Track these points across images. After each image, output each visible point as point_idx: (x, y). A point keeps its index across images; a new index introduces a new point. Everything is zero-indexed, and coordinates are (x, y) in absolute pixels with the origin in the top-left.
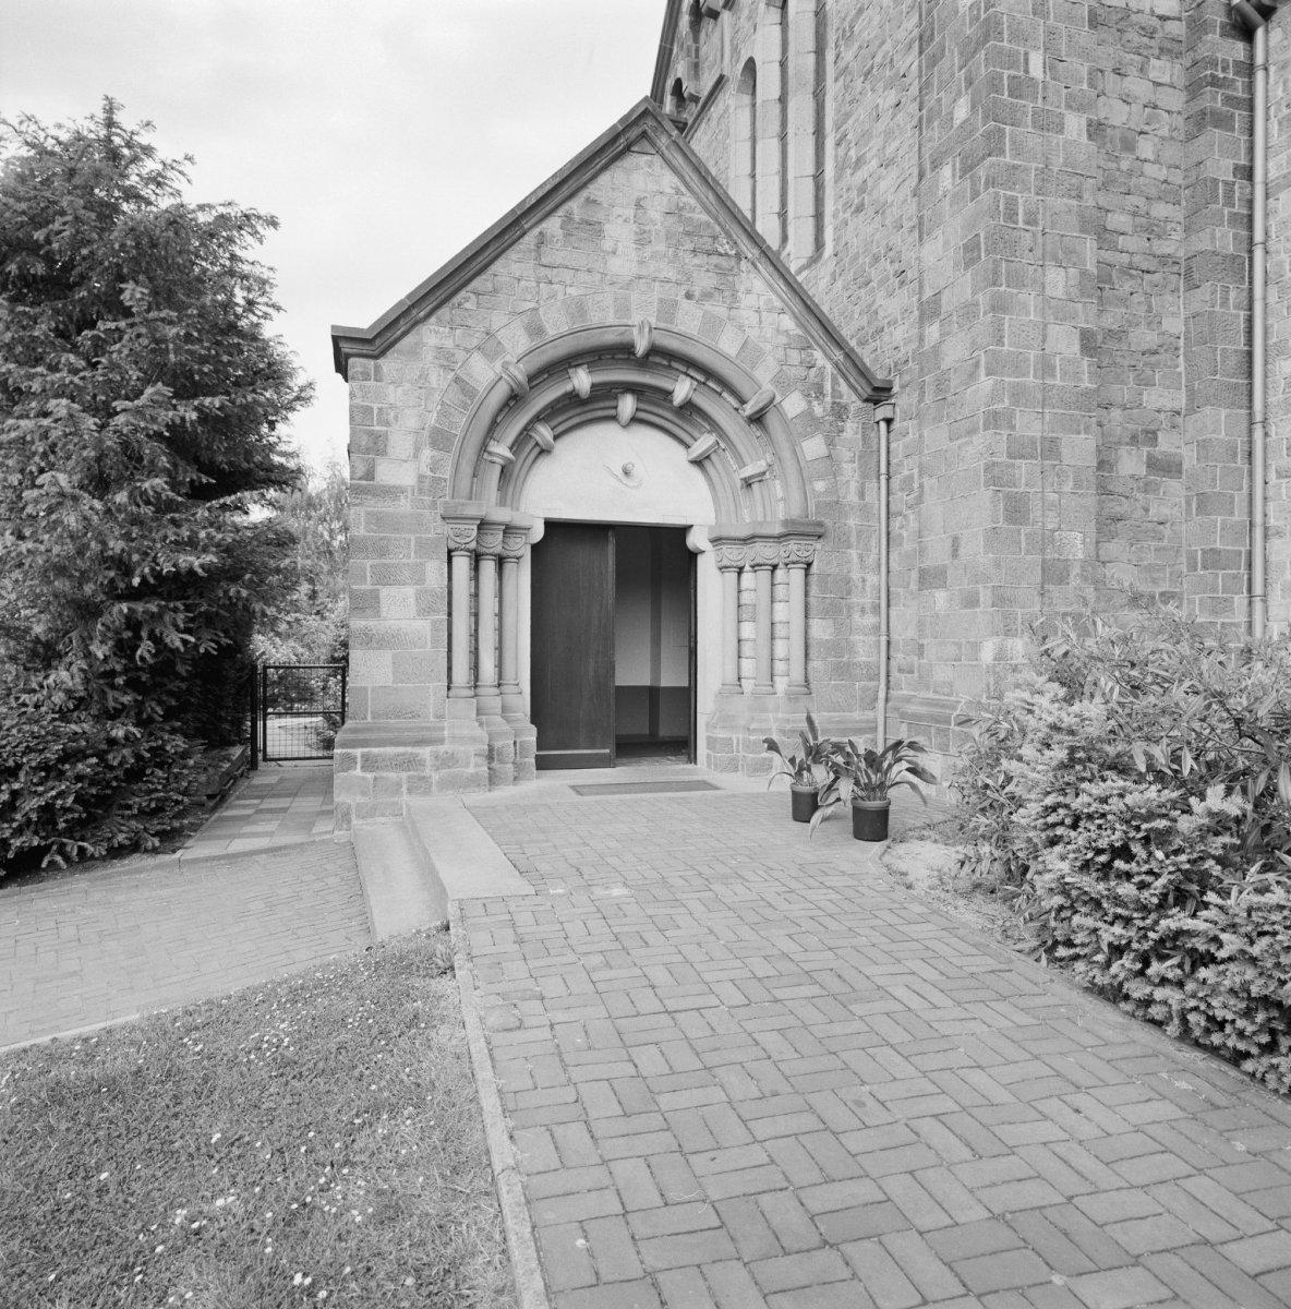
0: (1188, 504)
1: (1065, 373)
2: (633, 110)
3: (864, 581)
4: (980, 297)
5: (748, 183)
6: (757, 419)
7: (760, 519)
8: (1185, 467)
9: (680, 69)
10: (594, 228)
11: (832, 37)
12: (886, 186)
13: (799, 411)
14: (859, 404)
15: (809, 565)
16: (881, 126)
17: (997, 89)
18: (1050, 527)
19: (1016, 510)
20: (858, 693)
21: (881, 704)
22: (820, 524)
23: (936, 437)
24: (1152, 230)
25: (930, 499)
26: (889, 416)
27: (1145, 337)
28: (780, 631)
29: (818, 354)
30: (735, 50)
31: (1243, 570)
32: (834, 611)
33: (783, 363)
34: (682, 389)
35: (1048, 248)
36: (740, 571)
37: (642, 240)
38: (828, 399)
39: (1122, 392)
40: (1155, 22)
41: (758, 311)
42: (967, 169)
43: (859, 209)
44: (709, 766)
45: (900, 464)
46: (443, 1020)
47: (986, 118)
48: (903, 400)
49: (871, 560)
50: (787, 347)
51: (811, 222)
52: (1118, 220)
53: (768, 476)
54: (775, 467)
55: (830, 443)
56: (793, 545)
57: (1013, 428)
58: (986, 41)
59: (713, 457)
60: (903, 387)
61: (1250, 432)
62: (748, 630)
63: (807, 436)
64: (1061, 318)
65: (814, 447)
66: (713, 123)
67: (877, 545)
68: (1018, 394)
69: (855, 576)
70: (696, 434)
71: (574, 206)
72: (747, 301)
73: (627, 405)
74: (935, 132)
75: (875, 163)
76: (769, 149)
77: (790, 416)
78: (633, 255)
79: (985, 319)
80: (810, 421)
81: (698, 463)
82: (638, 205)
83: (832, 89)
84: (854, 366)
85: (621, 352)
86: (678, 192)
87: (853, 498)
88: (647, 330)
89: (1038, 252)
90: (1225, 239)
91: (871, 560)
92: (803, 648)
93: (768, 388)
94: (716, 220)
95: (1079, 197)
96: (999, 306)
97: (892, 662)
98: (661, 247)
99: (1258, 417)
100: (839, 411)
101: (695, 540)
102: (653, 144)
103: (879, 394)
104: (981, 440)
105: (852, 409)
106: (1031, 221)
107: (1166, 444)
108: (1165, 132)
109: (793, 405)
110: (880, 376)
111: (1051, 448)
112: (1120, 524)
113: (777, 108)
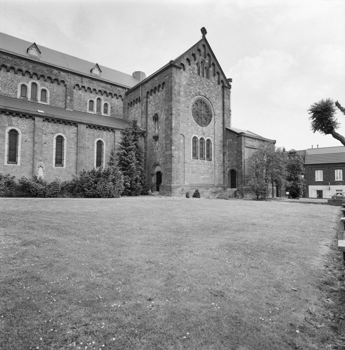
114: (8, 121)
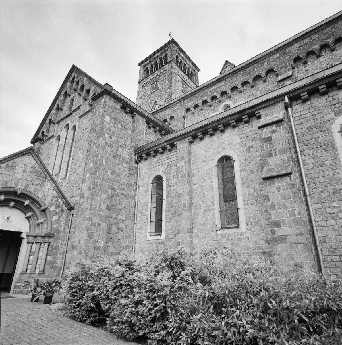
0: (124, 236)
1: (103, 212)
2: (29, 148)
3: (62, 247)
4: (90, 196)
5: (54, 158)
6: (44, 211)
7: (40, 232)
8: (124, 230)
9: (44, 129)
10: (13, 168)
11: (75, 141)
12: (79, 170)
13: (53, 210)
14: (67, 210)
15: (49, 243)
16: (80, 160)
17: (97, 164)
18: (97, 239)
19: (91, 236)
20: (56, 273)
21: (60, 276)
22: (54, 234)
23: (79, 220)
24: (121, 189)
25: (76, 232)
26: (73, 213)
27: (119, 207)
28: (40, 258)
29: (60, 199)
30: (57, 132)
31: (131, 249)
32: (53, 254)
33: (52, 200)
34: (27, 202)
35: (103, 190)
36: (33, 243)
37: (24, 171)
38: (60, 208)
39: (114, 216)
40: (125, 158)
41: (48, 189)
42: (91, 175)
43: (74, 172)
44: (13, 293)
45: (73, 223)
46: (133, 117)
47: (95, 168)
48: (76, 211)
49: (64, 243)
50: (53, 197)
51: (66, 170)
52: (116, 187)
53: (44, 223)
54: (46, 221)
55: (59, 217)
56: (46, 239)
57: (92, 220)
58: (96, 156)
59: (32, 217)
60: (76, 208)
61: (134, 225)
62: (31, 258)
63: (54, 215)
64: (104, 202)
65: (55, 218)
66: (50, 143)
67: (66, 241)
68: (94, 215)
69: (60, 246)
70: (28, 212)
71: (10, 163)
72: (46, 187)
73: (12, 204)
74: (87, 166)
75: (78, 166)
76: (60, 154)
77: (51, 211)
78: (22, 174)
79: (90, 201)
80: (55, 213)
81: (28, 218)
82: (25, 165)
83: (73, 149)
84: (67, 203)
85: (14, 193)
86: (35, 164)
87: (62, 229)
88: (21, 190)
89: (101, 191)
90: (132, 193)
91: (64, 243)
92: (44, 261)
93: (47, 205)
94: (42, 171)
95: (109, 183)
96: (93, 199)
97: (65, 266)
98: (29, 174)
99: (135, 223)
100: (62, 211)
101: (24, 235)
102: (32, 154)
103: (71, 209)
104: (87, 222)
105: (65, 211)
106: (100, 185)
107: (121, 225)
108: (125, 175)
109: (52, 209)
110: (72, 205)
111: (99, 225)
112: (111, 239)
113: (63, 146)
114: (332, 105)
